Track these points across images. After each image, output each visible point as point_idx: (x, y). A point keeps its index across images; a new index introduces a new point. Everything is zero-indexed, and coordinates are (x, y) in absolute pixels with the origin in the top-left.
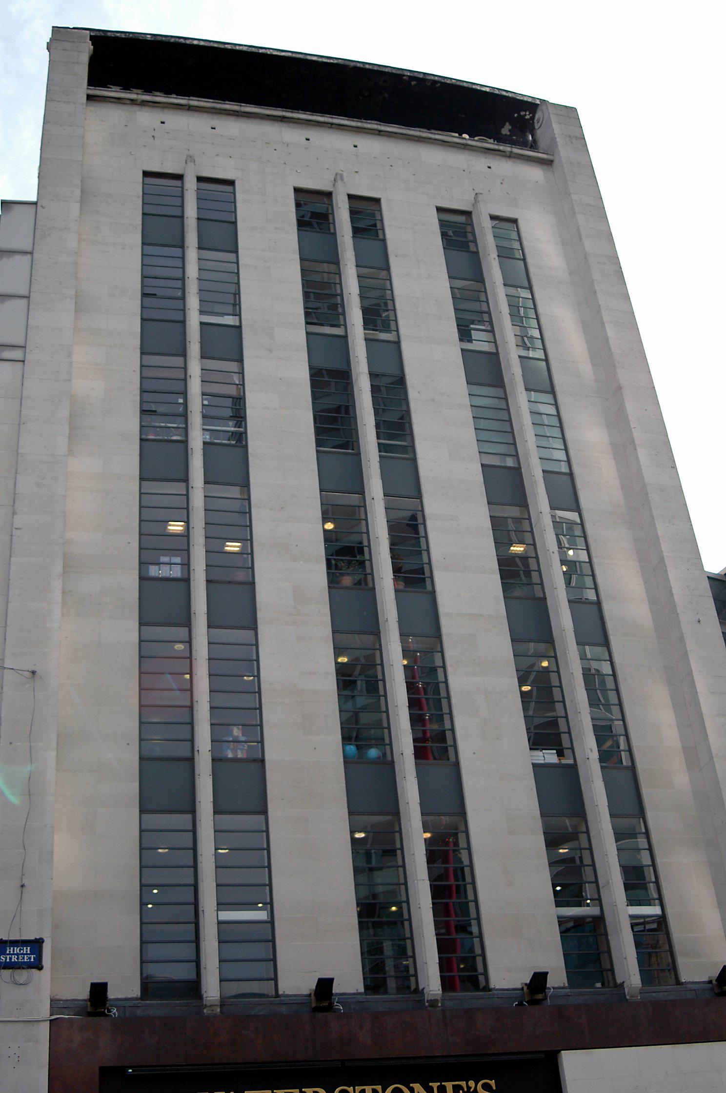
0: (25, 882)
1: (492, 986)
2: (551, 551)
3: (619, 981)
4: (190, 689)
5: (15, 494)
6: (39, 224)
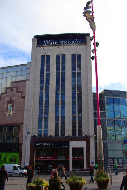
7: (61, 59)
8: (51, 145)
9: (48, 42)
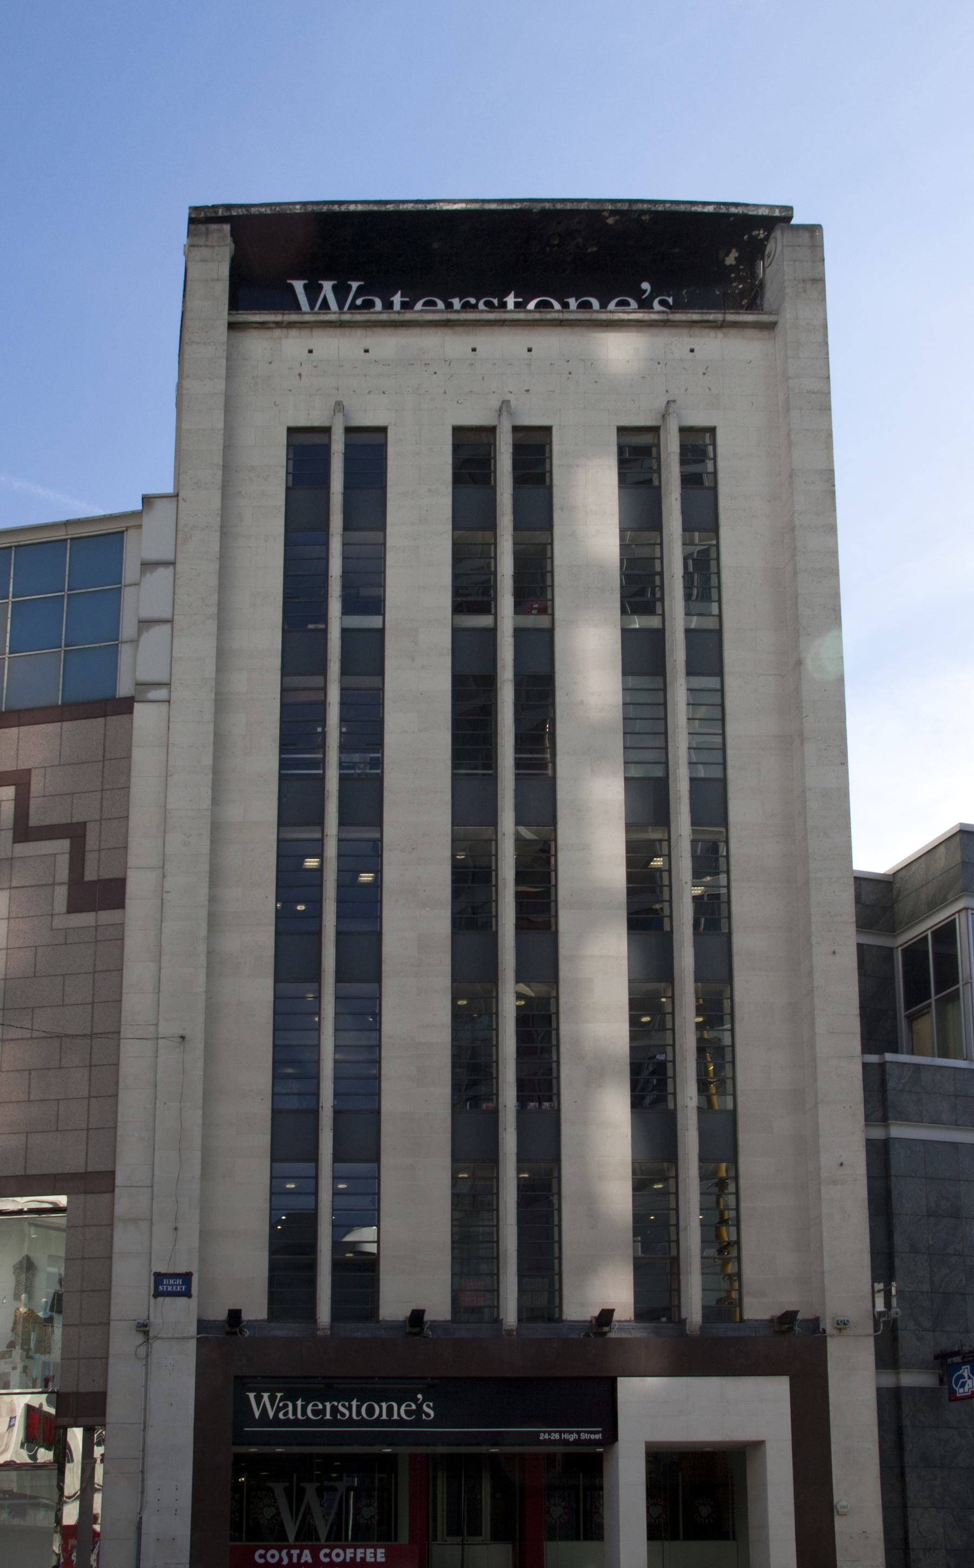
0: (179, 1226)
1: (564, 1318)
2: (684, 881)
3: (683, 1316)
4: (317, 1094)
5: (164, 855)
6: (181, 523)
7: (502, 472)
8: (418, 1422)
9: (272, 1399)
